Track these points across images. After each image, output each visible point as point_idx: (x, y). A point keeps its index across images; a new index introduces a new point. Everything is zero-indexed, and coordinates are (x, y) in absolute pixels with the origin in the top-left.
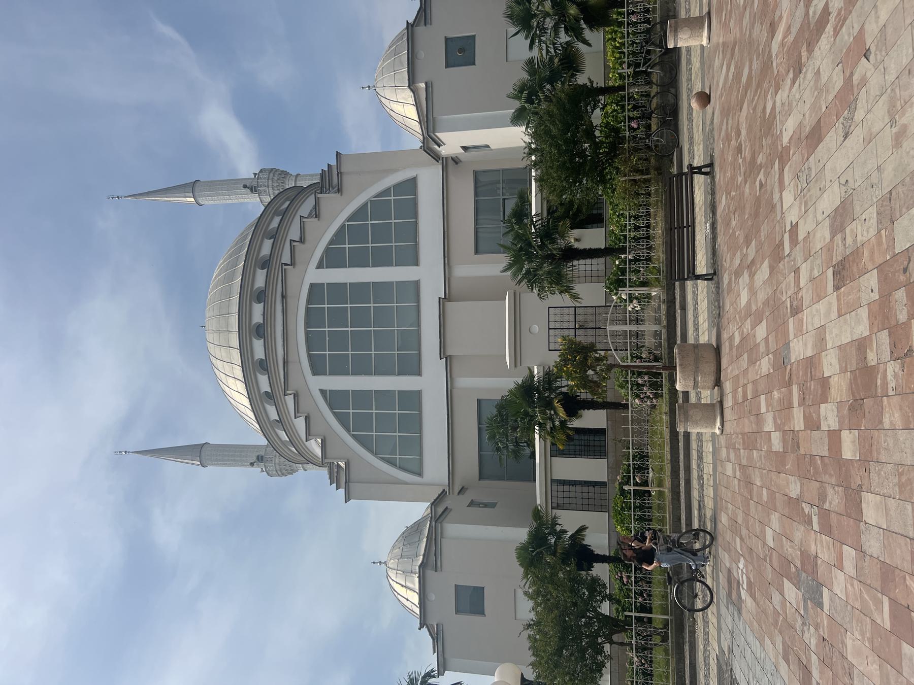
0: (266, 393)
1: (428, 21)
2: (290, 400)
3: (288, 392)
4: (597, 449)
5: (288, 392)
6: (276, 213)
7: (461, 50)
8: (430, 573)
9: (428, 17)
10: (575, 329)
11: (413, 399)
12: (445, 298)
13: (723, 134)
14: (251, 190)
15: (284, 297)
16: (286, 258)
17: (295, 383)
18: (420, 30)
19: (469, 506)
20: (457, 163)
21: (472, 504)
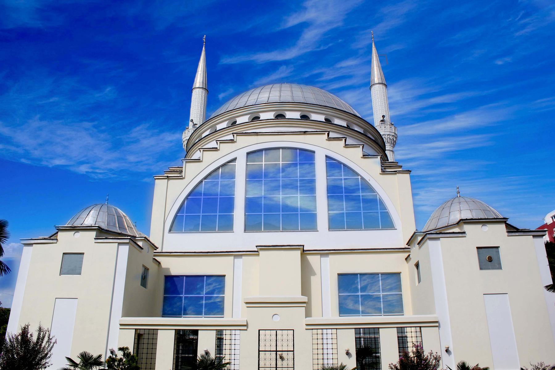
0: (236, 122)
1: (511, 234)
2: (231, 137)
3: (235, 135)
4: (150, 341)
5: (235, 135)
6: (365, 130)
7: (490, 259)
8: (93, 234)
9: (513, 234)
10: (276, 351)
11: (227, 225)
12: (304, 251)
13: (307, 185)
14: (382, 121)
15: (305, 133)
16: (332, 135)
17: (241, 140)
18: (502, 227)
19: (143, 266)
20: (406, 259)
21: (146, 269)
